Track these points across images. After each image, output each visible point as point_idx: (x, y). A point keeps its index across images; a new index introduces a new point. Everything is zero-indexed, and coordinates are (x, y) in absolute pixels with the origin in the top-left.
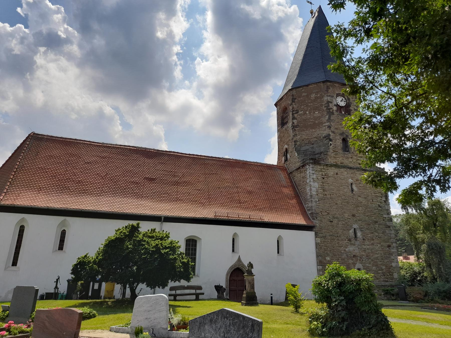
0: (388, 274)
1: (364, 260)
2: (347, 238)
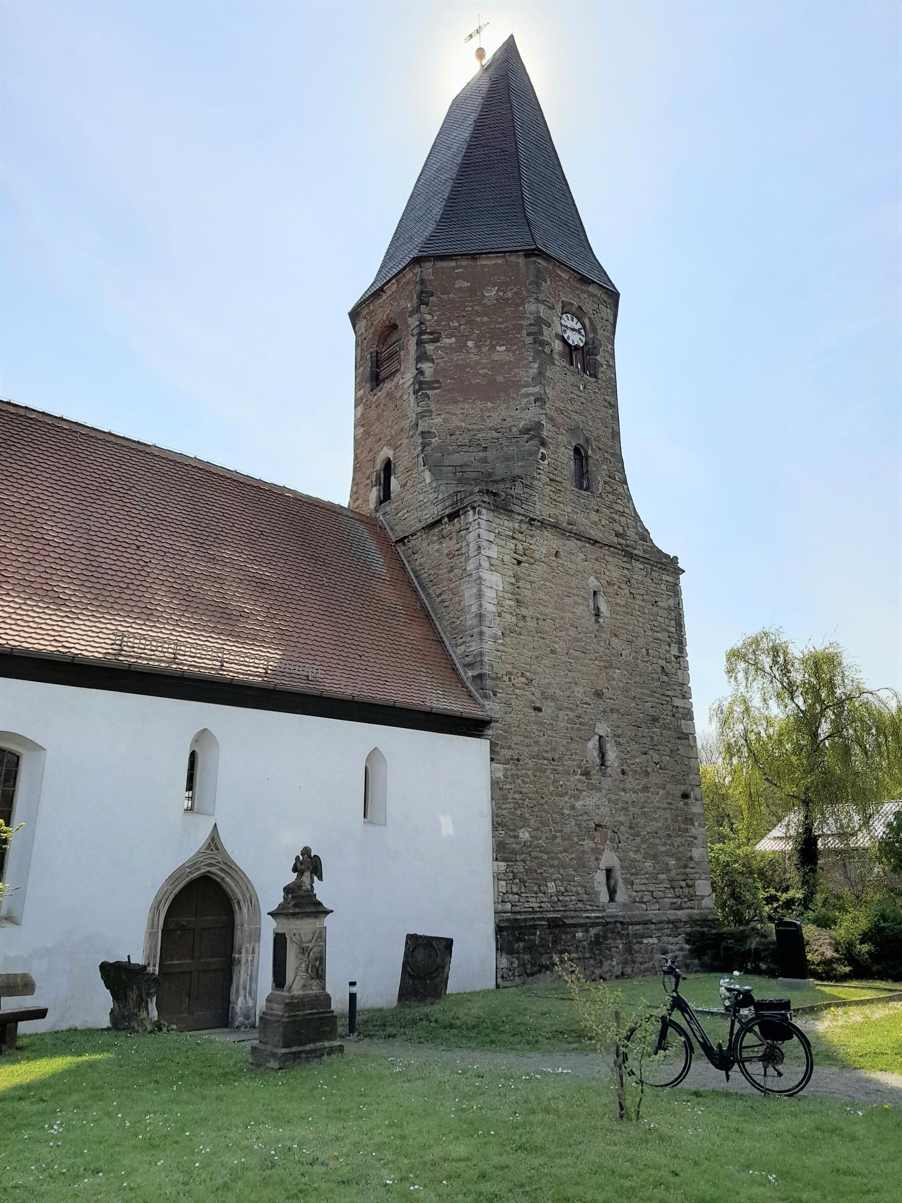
0: (683, 884)
1: (623, 838)
2: (580, 767)
